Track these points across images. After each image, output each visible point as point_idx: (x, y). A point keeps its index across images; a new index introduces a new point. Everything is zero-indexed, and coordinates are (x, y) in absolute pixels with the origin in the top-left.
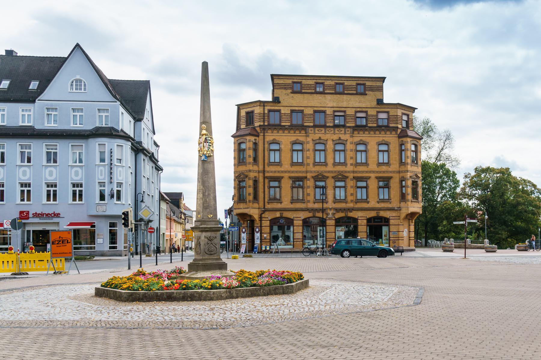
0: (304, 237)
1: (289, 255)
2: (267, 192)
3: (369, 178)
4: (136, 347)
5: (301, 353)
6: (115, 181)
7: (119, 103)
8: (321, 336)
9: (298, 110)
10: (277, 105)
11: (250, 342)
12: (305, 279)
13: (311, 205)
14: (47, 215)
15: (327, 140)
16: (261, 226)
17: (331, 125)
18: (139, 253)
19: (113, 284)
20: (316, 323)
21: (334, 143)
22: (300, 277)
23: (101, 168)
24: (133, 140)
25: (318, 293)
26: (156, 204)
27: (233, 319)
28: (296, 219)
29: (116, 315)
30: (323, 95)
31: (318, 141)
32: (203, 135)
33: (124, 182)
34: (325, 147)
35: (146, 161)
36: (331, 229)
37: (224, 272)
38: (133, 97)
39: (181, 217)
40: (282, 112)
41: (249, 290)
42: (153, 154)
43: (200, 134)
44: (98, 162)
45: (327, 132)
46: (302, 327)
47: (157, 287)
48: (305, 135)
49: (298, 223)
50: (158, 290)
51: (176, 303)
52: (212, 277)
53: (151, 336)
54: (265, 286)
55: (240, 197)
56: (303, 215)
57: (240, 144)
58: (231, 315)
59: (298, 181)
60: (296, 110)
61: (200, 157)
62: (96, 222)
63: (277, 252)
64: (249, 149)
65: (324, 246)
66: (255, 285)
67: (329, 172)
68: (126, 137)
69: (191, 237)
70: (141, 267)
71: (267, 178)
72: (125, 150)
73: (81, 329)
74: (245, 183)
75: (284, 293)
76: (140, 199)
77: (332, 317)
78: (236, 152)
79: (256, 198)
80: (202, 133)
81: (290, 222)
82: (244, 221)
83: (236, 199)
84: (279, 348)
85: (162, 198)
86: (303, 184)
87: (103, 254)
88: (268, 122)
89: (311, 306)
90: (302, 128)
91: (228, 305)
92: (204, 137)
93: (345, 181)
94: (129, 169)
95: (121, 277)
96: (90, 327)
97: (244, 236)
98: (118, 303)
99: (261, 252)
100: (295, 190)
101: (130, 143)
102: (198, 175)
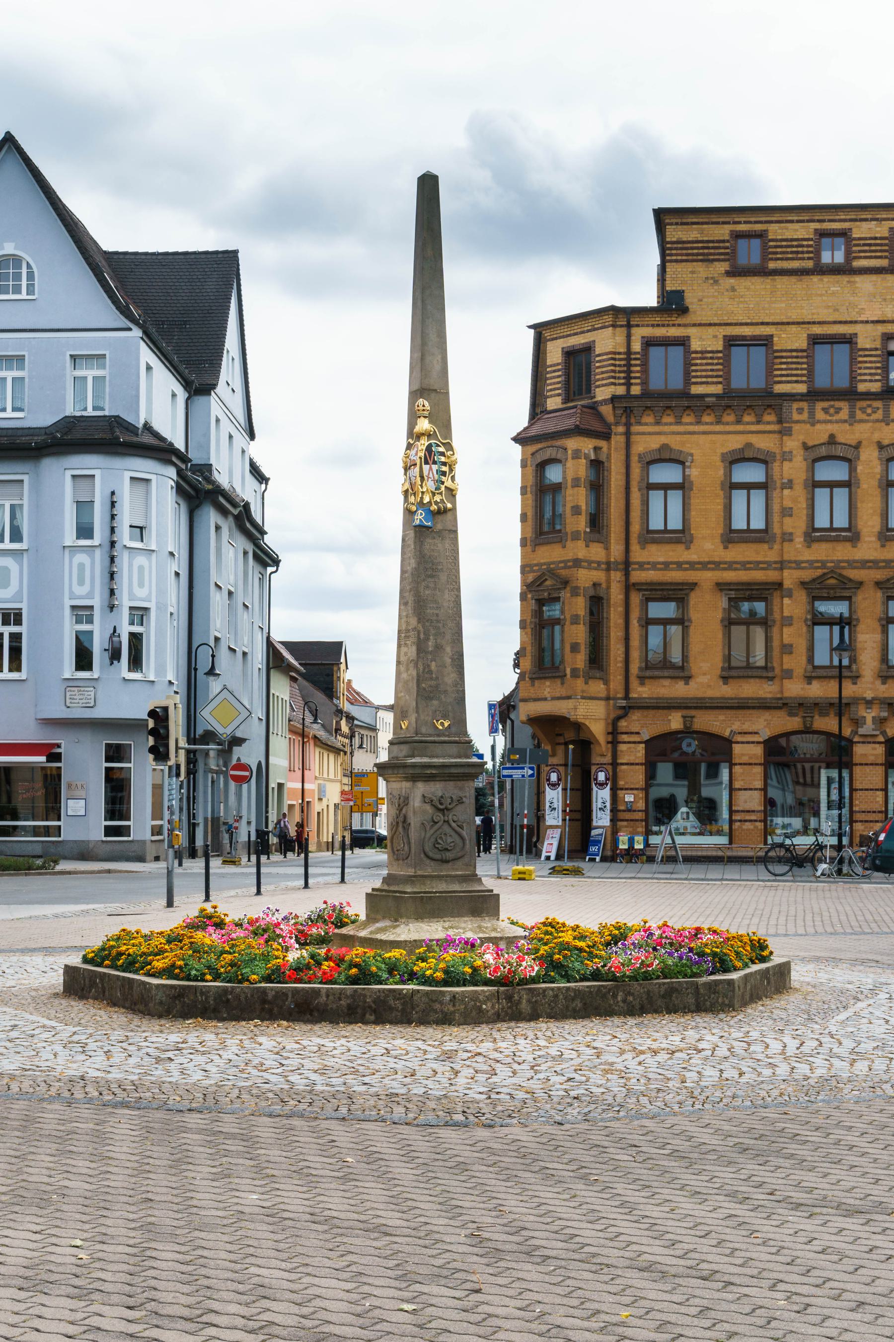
0: (770, 803)
1: (715, 871)
2: (635, 642)
3: (693, 586)
4: (201, 1173)
5: (767, 1229)
6: (125, 602)
7: (137, 333)
8: (837, 1173)
9: (754, 338)
10: (675, 320)
11: (584, 1177)
12: (776, 960)
13: (794, 689)
15: (857, 446)
16: (615, 764)
17: (876, 387)
18: (200, 852)
19: (120, 954)
20: (819, 1121)
21: (886, 455)
22: (759, 950)
23: (81, 558)
24: (184, 458)
25: (827, 1013)
26: (257, 682)
27: (521, 1095)
28: (739, 738)
29: (132, 1061)
30: (845, 279)
31: (823, 451)
32: (419, 436)
33: (152, 605)
34: (852, 470)
35: (225, 531)
36: (868, 776)
37: (487, 923)
38: (184, 307)
39: (338, 729)
40: (695, 345)
41: (577, 991)
42: (247, 506)
43: (411, 434)
44: (70, 537)
45: (859, 415)
46: (767, 1137)
47: (262, 969)
48: (776, 427)
49: (748, 752)
50: (268, 979)
51: (325, 1027)
52: (448, 943)
53: (248, 1140)
54: (634, 978)
55: (540, 658)
56: (766, 725)
57: (541, 466)
58: (514, 1080)
59: (750, 599)
60: (744, 338)
61: (409, 513)
62: (66, 743)
63: (670, 859)
64: (576, 483)
65: (845, 841)
66: (596, 975)
67: (864, 564)
68: (160, 450)
69: (371, 800)
70: (207, 899)
71: (639, 587)
72: (150, 498)
73: (22, 1104)
74: (558, 607)
75: (700, 1008)
76: (204, 665)
77: (879, 1104)
79: (597, 659)
80: (417, 429)
81: (719, 750)
82: (555, 744)
83: (527, 663)
84: (687, 1205)
85: (275, 659)
86: (769, 610)
87: (84, 853)
88: (645, 383)
89: (799, 1058)
90: (765, 402)
91: (503, 1045)
92: (424, 442)
93: (849, 599)
94: (169, 559)
95: (145, 931)
96: (51, 1100)
97: (554, 797)
98: (136, 1021)
99: (612, 856)
100: (738, 631)
101: (172, 472)
102: (402, 579)
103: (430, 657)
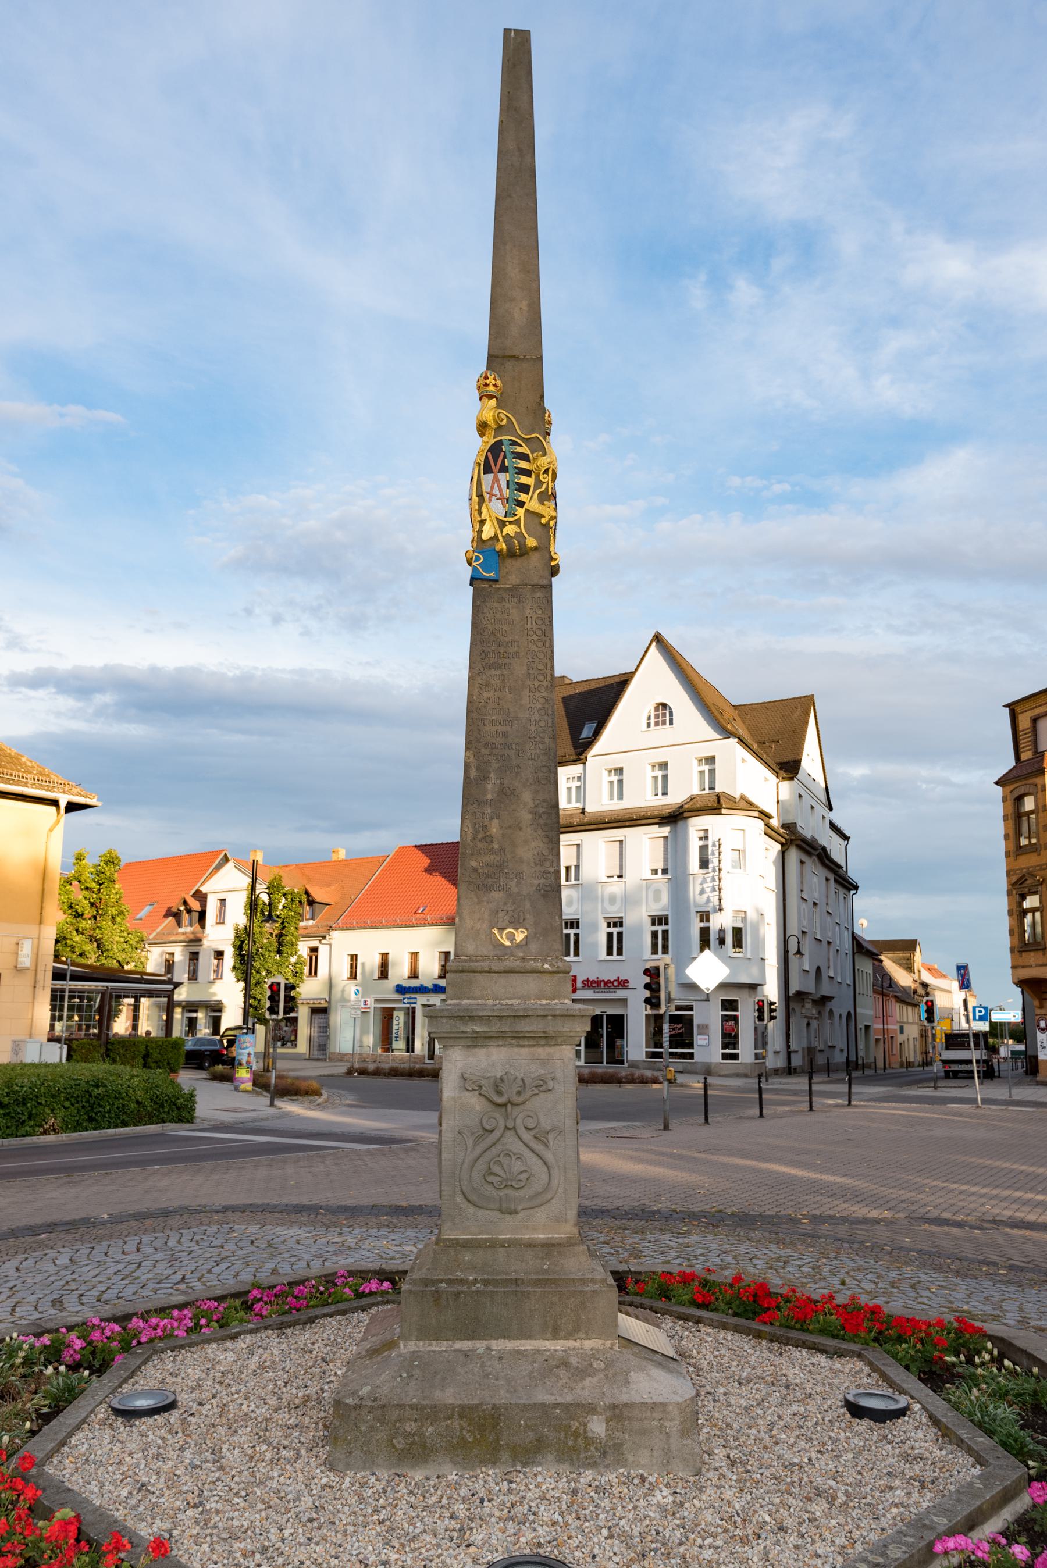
14: (606, 983)
78: (1011, 822)
103: (488, 811)
